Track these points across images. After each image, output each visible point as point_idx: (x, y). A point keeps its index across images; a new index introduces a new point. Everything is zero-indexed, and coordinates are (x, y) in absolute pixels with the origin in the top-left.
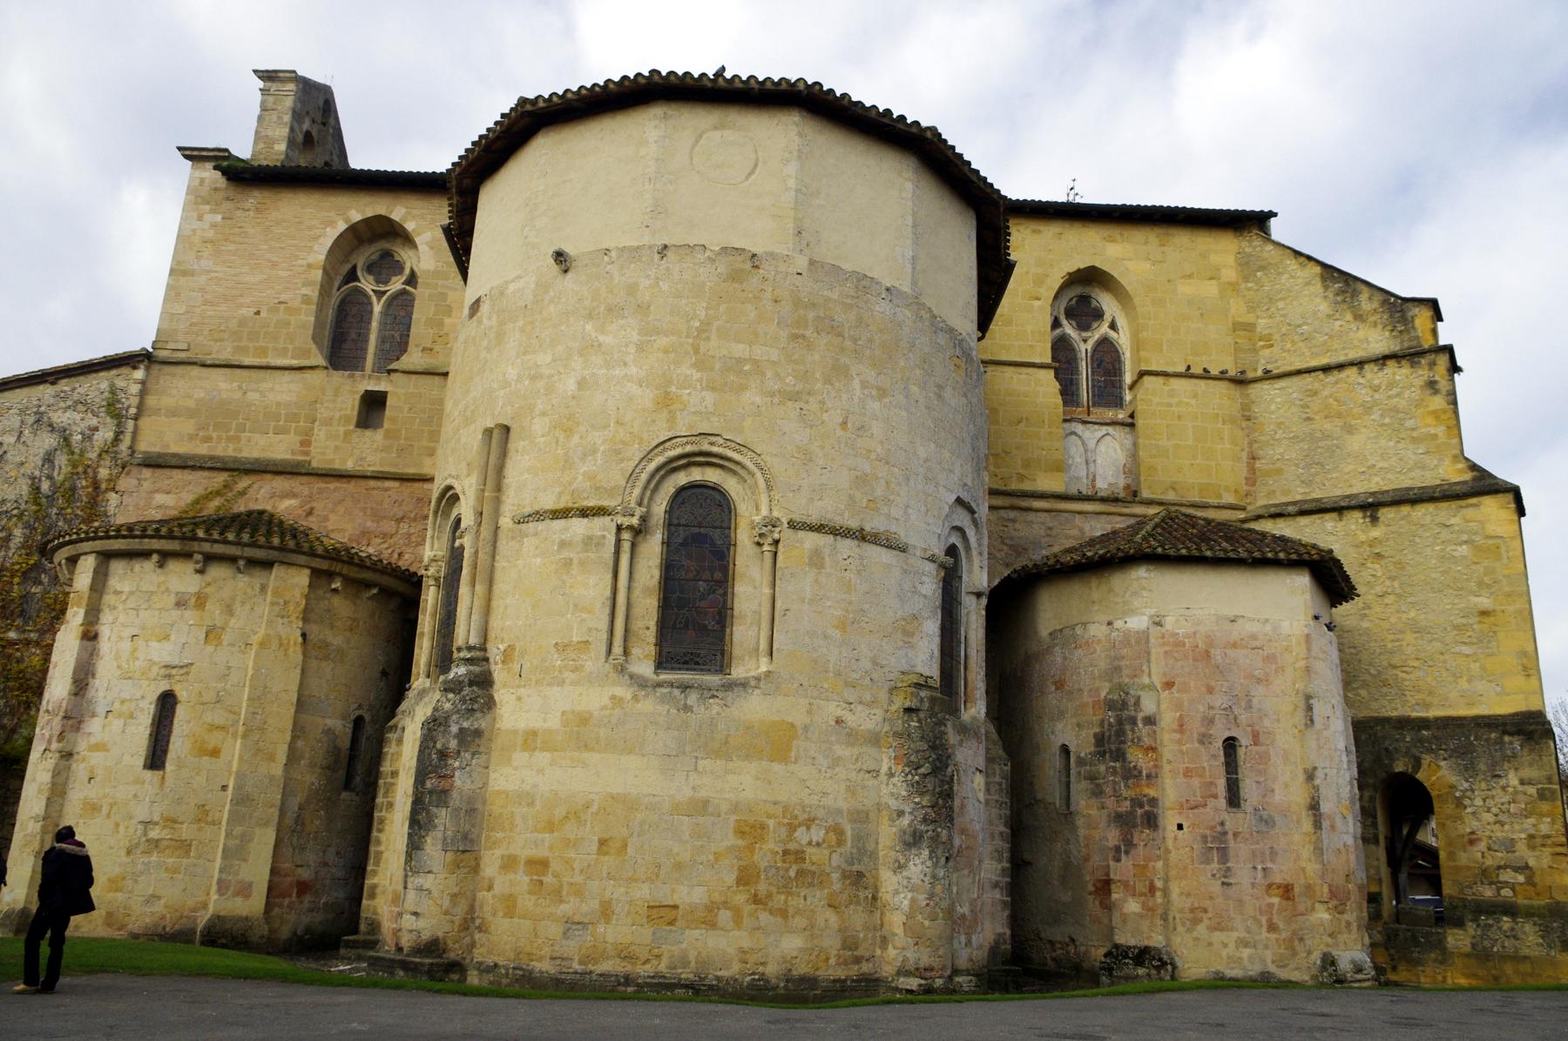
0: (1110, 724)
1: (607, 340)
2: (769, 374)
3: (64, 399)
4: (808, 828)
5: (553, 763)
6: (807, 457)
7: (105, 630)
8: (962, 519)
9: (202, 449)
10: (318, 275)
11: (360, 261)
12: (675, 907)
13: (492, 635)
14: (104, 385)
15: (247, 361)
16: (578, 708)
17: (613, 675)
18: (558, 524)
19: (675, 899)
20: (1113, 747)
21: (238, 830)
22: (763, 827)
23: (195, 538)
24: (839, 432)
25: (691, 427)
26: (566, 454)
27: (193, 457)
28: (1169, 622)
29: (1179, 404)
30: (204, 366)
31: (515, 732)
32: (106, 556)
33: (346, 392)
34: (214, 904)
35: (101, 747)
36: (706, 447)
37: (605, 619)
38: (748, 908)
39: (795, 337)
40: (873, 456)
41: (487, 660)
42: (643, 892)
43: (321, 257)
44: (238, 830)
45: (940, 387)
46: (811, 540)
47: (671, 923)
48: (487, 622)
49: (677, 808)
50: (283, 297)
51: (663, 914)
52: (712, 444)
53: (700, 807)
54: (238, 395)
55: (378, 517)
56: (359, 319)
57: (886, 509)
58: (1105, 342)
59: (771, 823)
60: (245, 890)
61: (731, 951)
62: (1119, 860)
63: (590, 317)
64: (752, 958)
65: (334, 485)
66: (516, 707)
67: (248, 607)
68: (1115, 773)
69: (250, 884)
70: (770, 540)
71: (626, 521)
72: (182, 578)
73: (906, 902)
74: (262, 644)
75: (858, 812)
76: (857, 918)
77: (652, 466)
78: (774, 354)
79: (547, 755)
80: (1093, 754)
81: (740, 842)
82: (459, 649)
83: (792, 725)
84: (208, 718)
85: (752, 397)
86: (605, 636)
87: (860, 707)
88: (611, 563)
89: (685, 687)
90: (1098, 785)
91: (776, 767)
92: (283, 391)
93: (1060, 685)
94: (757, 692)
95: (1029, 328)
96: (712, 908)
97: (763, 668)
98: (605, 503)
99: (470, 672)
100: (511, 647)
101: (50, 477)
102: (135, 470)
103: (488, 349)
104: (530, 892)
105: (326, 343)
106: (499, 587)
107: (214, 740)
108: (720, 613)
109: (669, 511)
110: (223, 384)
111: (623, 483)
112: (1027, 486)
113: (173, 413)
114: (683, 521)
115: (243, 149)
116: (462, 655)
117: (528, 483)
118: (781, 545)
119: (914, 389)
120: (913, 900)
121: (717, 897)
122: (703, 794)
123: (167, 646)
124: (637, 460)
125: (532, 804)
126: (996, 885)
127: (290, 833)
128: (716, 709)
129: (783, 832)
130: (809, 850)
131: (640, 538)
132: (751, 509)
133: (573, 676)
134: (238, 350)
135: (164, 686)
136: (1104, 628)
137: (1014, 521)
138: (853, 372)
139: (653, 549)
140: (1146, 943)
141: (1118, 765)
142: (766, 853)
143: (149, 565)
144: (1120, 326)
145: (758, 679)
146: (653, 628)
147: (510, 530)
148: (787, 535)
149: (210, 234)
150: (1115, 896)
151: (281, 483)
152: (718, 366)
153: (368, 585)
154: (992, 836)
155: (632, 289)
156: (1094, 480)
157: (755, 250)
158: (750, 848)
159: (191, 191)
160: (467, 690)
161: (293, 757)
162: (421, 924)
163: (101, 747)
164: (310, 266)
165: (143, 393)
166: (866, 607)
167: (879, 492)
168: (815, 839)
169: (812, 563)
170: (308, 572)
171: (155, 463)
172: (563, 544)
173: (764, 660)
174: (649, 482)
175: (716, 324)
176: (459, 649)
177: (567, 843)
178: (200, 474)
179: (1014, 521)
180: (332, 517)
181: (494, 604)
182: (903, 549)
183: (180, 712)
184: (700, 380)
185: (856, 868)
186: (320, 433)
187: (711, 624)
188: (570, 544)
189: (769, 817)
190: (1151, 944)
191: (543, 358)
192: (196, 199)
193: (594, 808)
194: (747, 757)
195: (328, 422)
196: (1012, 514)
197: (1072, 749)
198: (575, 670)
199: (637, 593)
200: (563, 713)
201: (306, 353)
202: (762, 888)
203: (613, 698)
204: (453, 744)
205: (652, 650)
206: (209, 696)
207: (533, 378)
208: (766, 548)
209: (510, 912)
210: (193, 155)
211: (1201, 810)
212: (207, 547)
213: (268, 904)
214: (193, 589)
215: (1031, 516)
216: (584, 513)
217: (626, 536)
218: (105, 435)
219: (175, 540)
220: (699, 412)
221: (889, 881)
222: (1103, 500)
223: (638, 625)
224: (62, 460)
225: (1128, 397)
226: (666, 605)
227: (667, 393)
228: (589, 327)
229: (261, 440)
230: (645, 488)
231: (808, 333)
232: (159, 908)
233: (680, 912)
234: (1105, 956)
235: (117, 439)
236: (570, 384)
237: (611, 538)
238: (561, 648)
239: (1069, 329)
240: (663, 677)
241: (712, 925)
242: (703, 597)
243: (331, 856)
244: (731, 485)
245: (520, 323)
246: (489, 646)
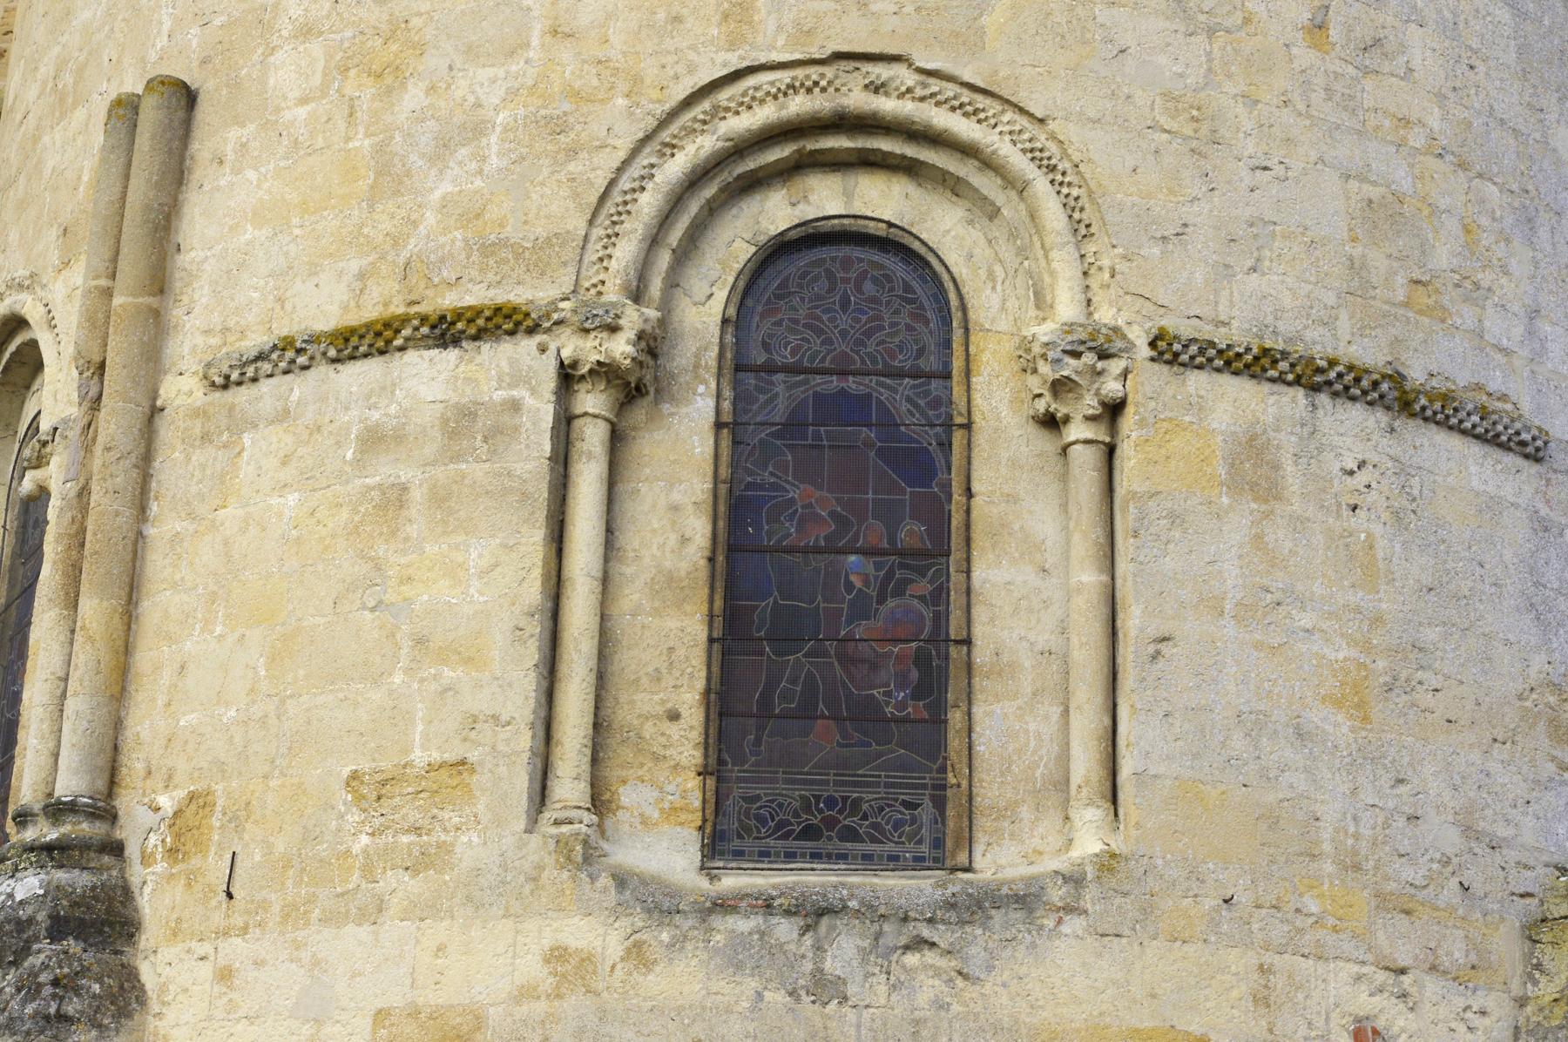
6: (1205, 137)
13: (134, 764)
16: (430, 997)
18: (367, 372)
24: (1304, 56)
26: (380, 149)
36: (857, 99)
37: (526, 684)
40: (1417, 139)
41: (116, 849)
46: (1233, 402)
48: (118, 725)
52: (877, 88)
57: (1467, 316)
70: (1090, 404)
71: (589, 350)
77: (676, 167)
82: (23, 818)
86: (524, 741)
87: (1433, 987)
88: (541, 492)
89: (815, 914)
94: (1073, 925)
99: (53, 892)
100: (199, 801)
106: (159, 604)
108: (922, 660)
109: (736, 323)
111: (578, 224)
114: (785, 356)
116: (30, 834)
117: (255, 256)
118: (1128, 421)
124: (623, 147)
128: (928, 989)
131: (639, 413)
132: (1013, 298)
133: (412, 885)
139: (683, 449)
145: (1074, 880)
147: (197, 413)
148: (1149, 387)
160: (43, 953)
166: (1431, 635)
167: (1443, 257)
169: (1238, 483)
172: (374, 440)
174: (666, 219)
176: (23, 818)
181: (144, 659)
187: (894, 700)
188: (399, 437)
199: (631, 596)
200: (381, 1016)
203: (557, 955)
205: (690, 789)
216: (446, 331)
217: (592, 401)
223: (637, 705)
226: (733, 635)
230: (654, 241)
237: (541, 409)
238: (374, 789)
240: (732, 881)
242: (860, 610)
244: (942, 226)
246: (127, 802)
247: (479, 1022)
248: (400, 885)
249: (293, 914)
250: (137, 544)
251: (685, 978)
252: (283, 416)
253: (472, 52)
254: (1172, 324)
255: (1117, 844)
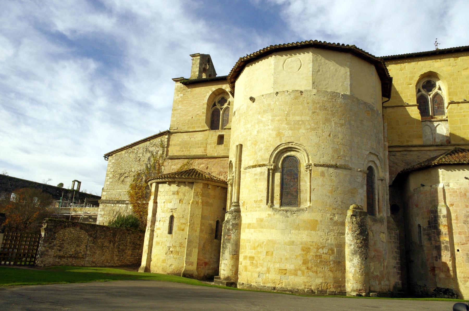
0: (432, 218)
1: (264, 119)
2: (307, 124)
3: (152, 144)
4: (323, 249)
5: (255, 232)
7: (158, 201)
8: (373, 158)
9: (181, 154)
10: (206, 106)
11: (217, 101)
12: (286, 270)
14: (159, 140)
15: (191, 130)
17: (268, 208)
18: (254, 169)
19: (286, 268)
20: (433, 225)
21: (189, 249)
22: (309, 248)
23: (175, 178)
25: (286, 141)
27: (180, 156)
28: (451, 185)
29: (464, 112)
30: (181, 133)
31: (246, 224)
32: (158, 183)
33: (215, 135)
34: (183, 266)
35: (159, 229)
38: (306, 271)
39: (314, 113)
42: (277, 266)
43: (206, 101)
44: (189, 249)
45: (362, 121)
46: (321, 169)
47: (285, 274)
49: (285, 243)
50: (198, 113)
51: (283, 272)
53: (292, 243)
54: (189, 139)
55: (224, 168)
56: (216, 116)
58: (437, 94)
59: (312, 247)
60: (192, 264)
61: (302, 282)
62: (437, 261)
63: (259, 114)
64: (307, 284)
65: (213, 160)
66: (247, 218)
67: (188, 194)
68: (434, 233)
69: (193, 262)
72: (174, 187)
73: (353, 270)
74: (192, 203)
75: (338, 245)
76: (339, 274)
78: (308, 118)
79: (253, 230)
80: (428, 227)
81: (303, 253)
83: (317, 221)
84: (181, 221)
85: (302, 131)
89: (287, 211)
90: (430, 237)
91: (313, 232)
92: (199, 137)
93: (417, 206)
95: (408, 94)
96: (296, 270)
97: (309, 205)
98: (265, 163)
101: (150, 164)
102: (167, 160)
103: (237, 124)
104: (250, 265)
105: (209, 123)
107: (183, 227)
110: (185, 136)
112: (410, 144)
113: (175, 145)
115: (188, 76)
117: (247, 160)
119: (352, 122)
120: (355, 270)
121: (297, 267)
122: (292, 240)
123: (171, 204)
125: (250, 242)
126: (395, 267)
127: (202, 250)
129: (315, 250)
130: (323, 255)
133: (258, 209)
134: (189, 128)
135: (171, 214)
136: (430, 187)
137: (406, 155)
138: (332, 120)
140: (447, 287)
141: (435, 230)
142: (310, 256)
143: (167, 185)
144: (443, 88)
145: (306, 208)
146: (279, 196)
148: (313, 168)
149: (180, 99)
150: (436, 272)
151: (200, 161)
152: (292, 123)
153: (218, 187)
154: (392, 252)
155: (269, 105)
156: (435, 139)
157: (301, 90)
158: (306, 254)
159: (176, 89)
160: (234, 213)
161: (201, 231)
162: (225, 273)
163: (159, 229)
164: (204, 104)
165: (168, 141)
168: (325, 252)
170: (202, 184)
171: (172, 158)
172: (255, 174)
173: (308, 203)
175: (291, 112)
177: (258, 252)
178: (181, 160)
179: (406, 155)
180: (213, 168)
182: (350, 169)
183: (175, 220)
184: (288, 128)
185: (338, 260)
186: (209, 147)
187: (295, 194)
189: (311, 246)
190: (450, 288)
191: (249, 126)
192: (178, 90)
193: (265, 244)
194: (304, 230)
195: (210, 144)
196: (405, 153)
197: (421, 225)
198: (259, 207)
201: (204, 126)
202: (310, 265)
203: (268, 214)
204: (231, 227)
206: (181, 216)
207: (247, 131)
208: (308, 172)
209: (246, 270)
210: (176, 80)
211: (465, 245)
212: (178, 180)
213: (197, 267)
214: (176, 190)
215: (412, 153)
216: (260, 166)
218: (160, 152)
219: (172, 179)
220: (288, 136)
221: (348, 265)
222: (437, 146)
224: (152, 159)
225: (446, 111)
227: (279, 132)
228: (259, 117)
229: (195, 150)
231: (317, 111)
232: (173, 267)
233: (288, 271)
234: (434, 291)
235: (163, 153)
236: (255, 132)
237: (267, 172)
238: (256, 202)
239: (423, 92)
241: (296, 275)
242: (292, 186)
243: (213, 256)
245: (244, 117)
246: (240, 202)
247: (263, 219)
248: (258, 209)
249: (251, 211)
250: (100, 293)
251: (278, 216)
252: (249, 172)
253: (261, 143)
254: (315, 163)
255: (311, 205)
